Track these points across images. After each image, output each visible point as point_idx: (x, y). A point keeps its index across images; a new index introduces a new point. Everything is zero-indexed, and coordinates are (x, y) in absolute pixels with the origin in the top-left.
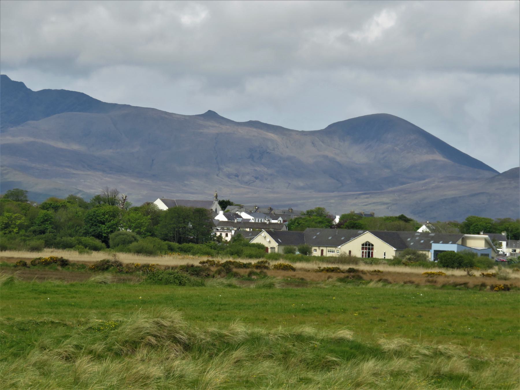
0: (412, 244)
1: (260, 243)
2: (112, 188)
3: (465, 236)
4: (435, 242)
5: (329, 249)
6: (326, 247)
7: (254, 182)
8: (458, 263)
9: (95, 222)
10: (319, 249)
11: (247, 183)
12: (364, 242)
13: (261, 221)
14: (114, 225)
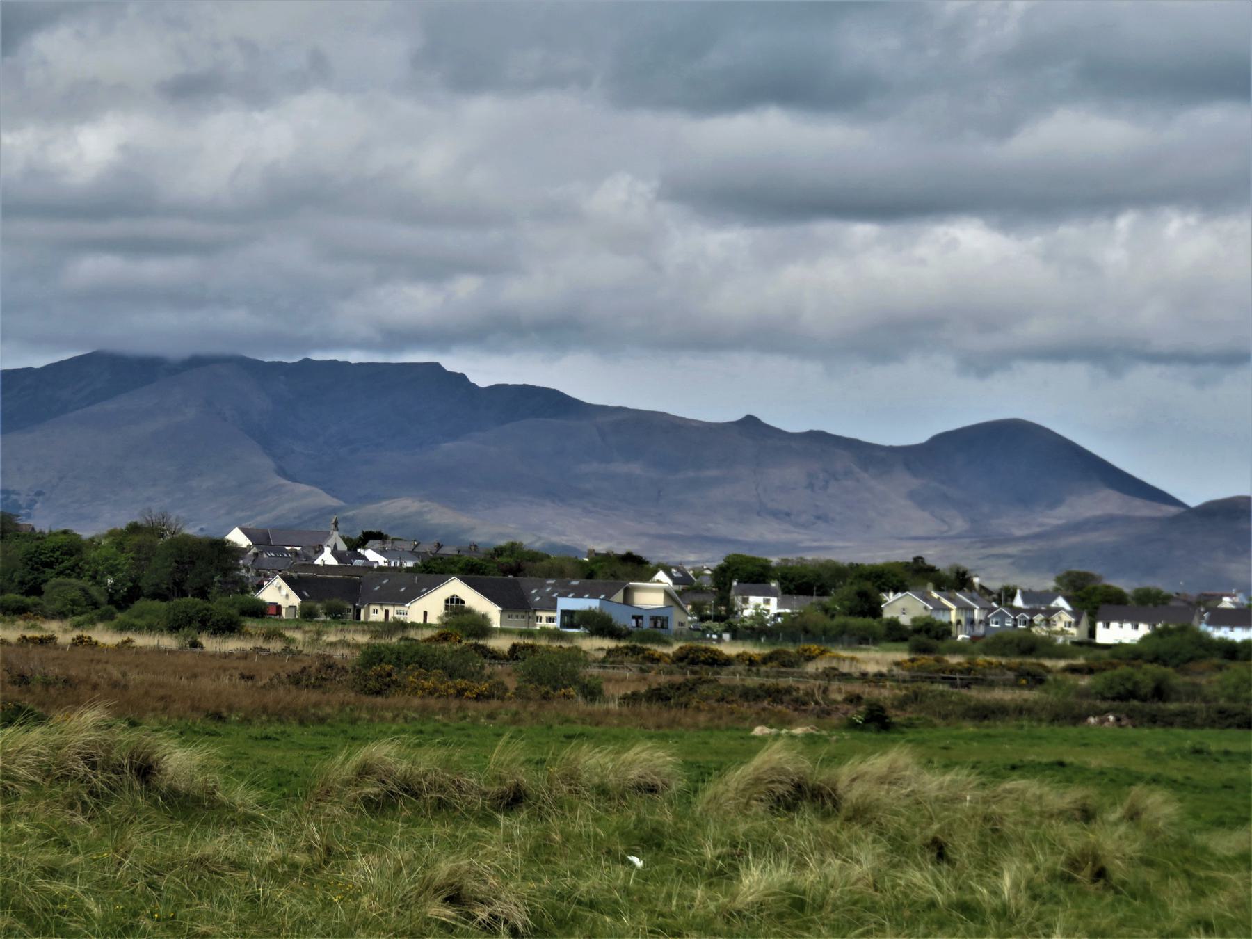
0: (537, 599)
1: (590, 608)
2: (156, 508)
3: (632, 586)
4: (561, 596)
5: (398, 608)
6: (394, 605)
7: (814, 524)
8: (199, 622)
9: (36, 563)
10: (382, 609)
11: (804, 526)
12: (448, 595)
13: (396, 564)
14: (68, 569)
